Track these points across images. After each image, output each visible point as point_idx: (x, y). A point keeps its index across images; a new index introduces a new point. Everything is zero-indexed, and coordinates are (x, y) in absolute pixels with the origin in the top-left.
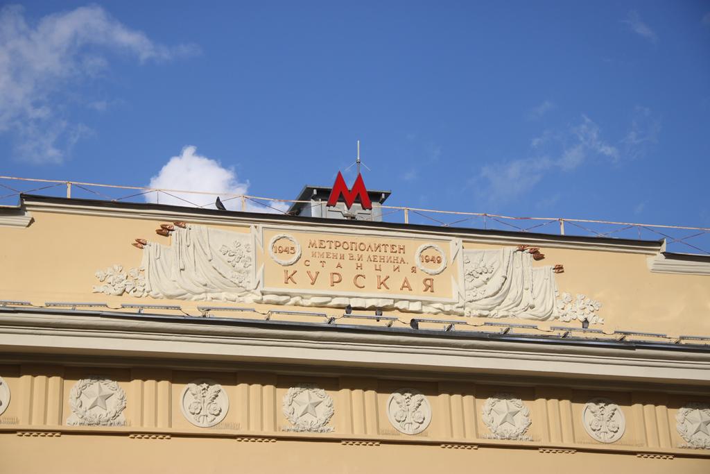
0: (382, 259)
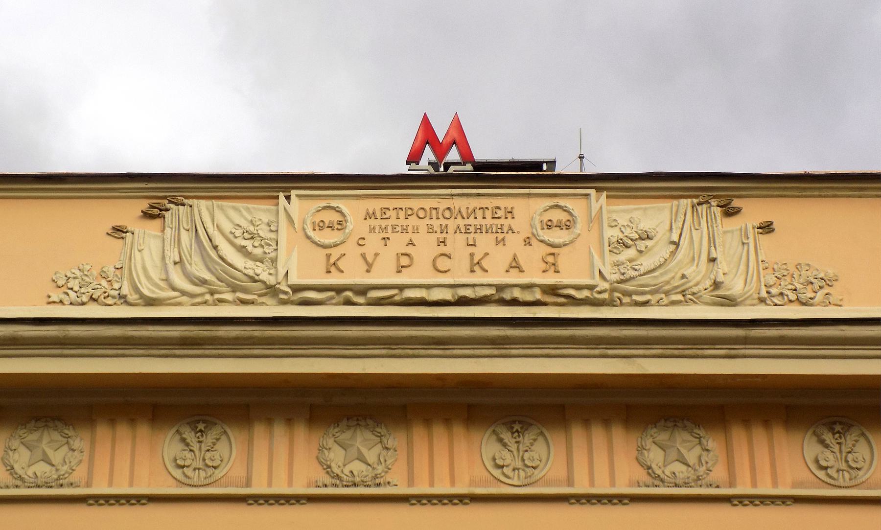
0: (479, 229)
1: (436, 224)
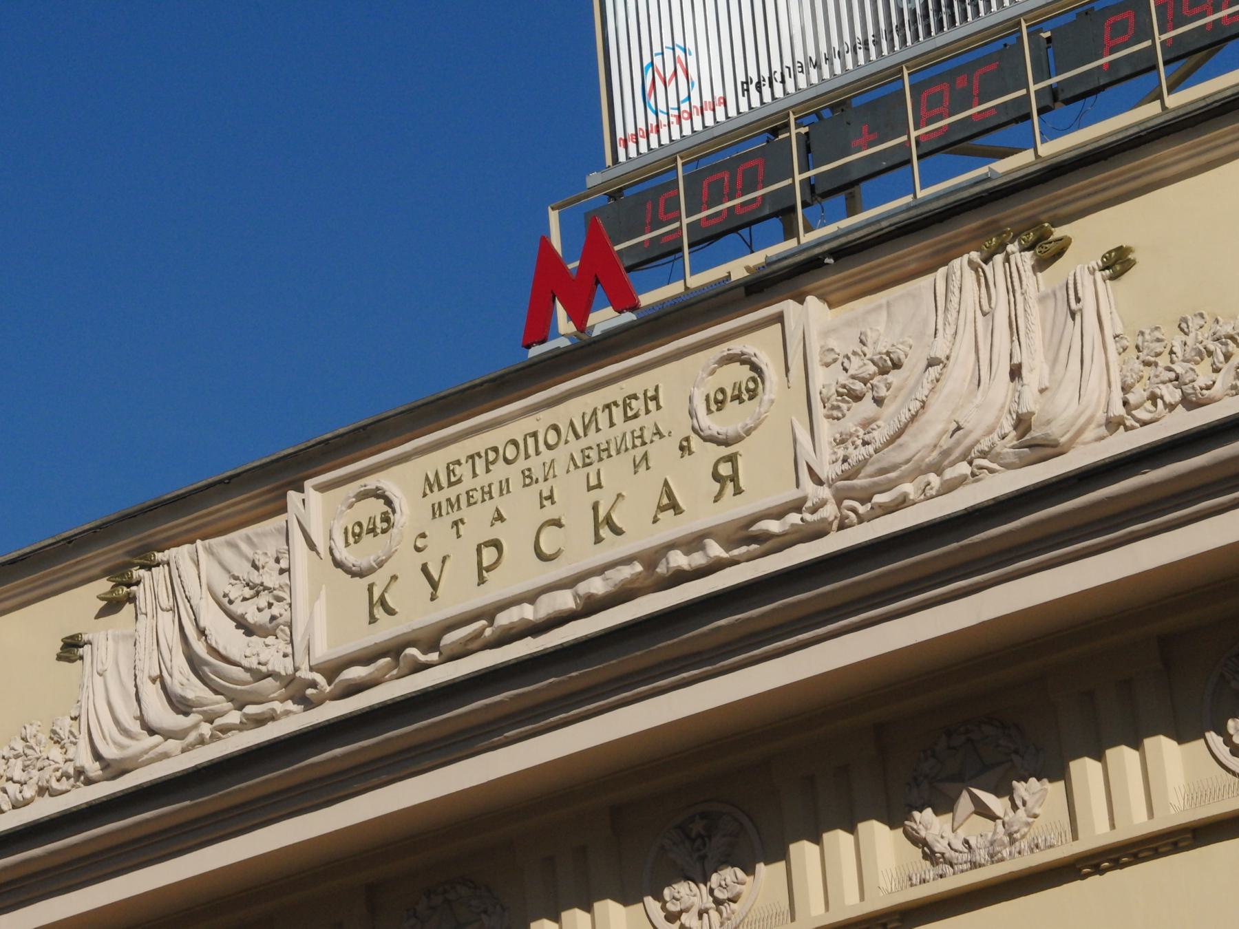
0: (604, 451)
1: (535, 463)
